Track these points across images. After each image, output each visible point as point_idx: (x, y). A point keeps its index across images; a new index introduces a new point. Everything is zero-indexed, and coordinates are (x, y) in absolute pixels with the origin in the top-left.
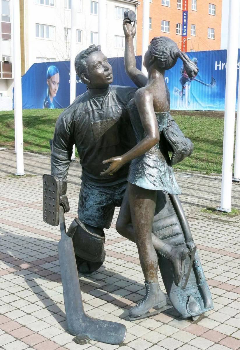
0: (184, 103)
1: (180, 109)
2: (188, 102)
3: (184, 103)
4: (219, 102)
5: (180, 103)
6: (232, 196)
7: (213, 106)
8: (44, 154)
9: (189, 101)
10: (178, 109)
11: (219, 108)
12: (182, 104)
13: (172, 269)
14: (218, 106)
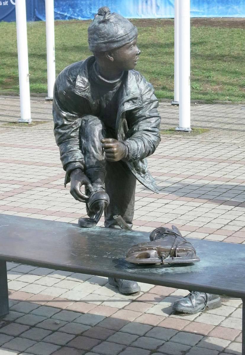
0: (149, 7)
1: (143, 17)
2: (157, 6)
3: (149, 7)
4: (207, 4)
5: (142, 8)
6: (191, 126)
7: (197, 10)
8: (9, 100)
9: (159, 4)
10: (141, 16)
11: (208, 14)
12: (147, 8)
13: (88, 255)
14: (206, 11)
